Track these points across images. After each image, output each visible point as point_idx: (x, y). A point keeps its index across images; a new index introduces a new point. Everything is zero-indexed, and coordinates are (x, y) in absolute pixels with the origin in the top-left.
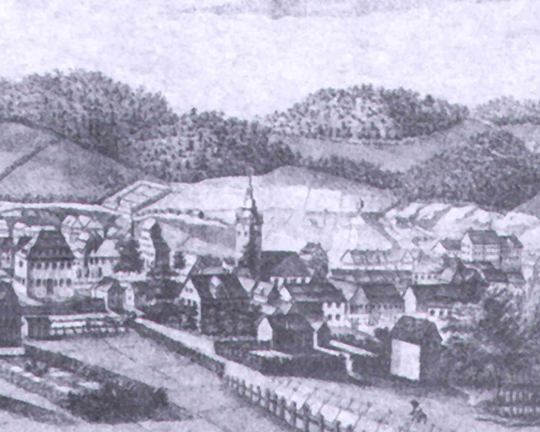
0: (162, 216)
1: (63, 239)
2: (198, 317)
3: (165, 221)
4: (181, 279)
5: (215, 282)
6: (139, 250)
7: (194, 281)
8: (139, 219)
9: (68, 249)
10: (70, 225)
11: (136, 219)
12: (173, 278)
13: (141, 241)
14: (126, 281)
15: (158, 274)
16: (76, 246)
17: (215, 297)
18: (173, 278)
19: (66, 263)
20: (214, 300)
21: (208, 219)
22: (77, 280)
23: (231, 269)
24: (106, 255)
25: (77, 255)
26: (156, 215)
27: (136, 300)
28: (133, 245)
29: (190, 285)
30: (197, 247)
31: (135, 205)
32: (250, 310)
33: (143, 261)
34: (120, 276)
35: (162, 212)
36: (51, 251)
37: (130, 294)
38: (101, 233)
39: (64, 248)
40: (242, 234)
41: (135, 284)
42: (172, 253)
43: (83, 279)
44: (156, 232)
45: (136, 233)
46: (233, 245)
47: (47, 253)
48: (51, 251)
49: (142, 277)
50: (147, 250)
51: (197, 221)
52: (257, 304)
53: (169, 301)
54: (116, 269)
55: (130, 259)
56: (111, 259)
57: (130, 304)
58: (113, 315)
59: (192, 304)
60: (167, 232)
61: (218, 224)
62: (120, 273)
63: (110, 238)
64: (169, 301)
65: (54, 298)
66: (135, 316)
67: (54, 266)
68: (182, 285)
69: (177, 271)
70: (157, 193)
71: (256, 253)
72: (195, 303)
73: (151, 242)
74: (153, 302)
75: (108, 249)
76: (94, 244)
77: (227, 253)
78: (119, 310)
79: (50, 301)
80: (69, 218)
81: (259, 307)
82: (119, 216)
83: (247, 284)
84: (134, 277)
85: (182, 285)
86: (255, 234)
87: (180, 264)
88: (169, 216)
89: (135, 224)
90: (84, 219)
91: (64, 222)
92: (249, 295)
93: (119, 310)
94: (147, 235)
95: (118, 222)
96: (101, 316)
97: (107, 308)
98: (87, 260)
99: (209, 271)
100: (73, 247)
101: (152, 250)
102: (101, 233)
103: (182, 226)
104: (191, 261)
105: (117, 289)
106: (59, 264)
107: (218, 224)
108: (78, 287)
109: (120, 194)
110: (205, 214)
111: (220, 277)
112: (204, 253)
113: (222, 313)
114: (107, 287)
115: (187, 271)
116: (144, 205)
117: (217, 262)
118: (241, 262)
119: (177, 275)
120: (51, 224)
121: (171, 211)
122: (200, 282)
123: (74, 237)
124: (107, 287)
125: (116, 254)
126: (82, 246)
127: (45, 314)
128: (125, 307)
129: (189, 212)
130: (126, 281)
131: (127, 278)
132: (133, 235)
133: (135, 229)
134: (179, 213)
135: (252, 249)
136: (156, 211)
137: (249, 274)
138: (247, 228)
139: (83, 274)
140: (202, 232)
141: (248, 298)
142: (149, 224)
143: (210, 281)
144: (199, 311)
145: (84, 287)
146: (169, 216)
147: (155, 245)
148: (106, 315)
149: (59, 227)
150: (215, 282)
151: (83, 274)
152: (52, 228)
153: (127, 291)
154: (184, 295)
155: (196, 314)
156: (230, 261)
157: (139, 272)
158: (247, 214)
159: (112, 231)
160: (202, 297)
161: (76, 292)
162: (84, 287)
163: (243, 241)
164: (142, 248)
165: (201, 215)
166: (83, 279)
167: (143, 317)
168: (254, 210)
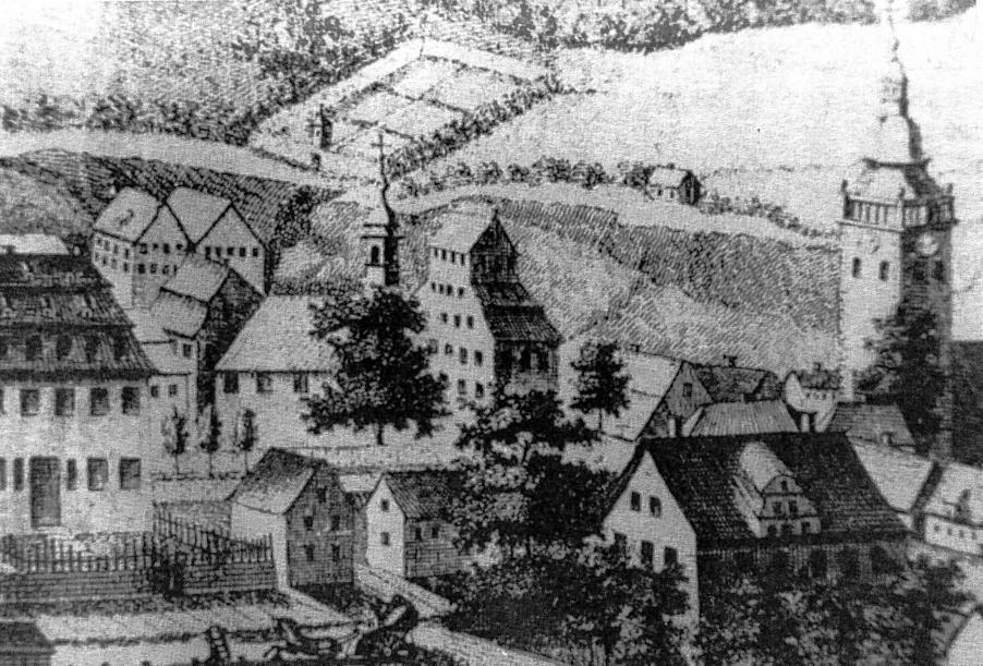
0: (520, 193)
1: (98, 288)
2: (688, 620)
3: (533, 214)
4: (609, 455)
5: (758, 465)
6: (419, 340)
7: (666, 468)
8: (423, 203)
9: (120, 334)
10: (132, 231)
11: (405, 207)
12: (572, 454)
13: (430, 303)
14: (366, 471)
15: (508, 435)
16: (156, 322)
17: (757, 528)
18: (572, 454)
19: (115, 389)
20: (753, 541)
21: (721, 206)
22: (167, 464)
23: (823, 408)
24: (276, 362)
25: (161, 357)
26: (489, 190)
27: (414, 550)
28: (392, 317)
29: (649, 480)
30: (682, 322)
31: (394, 143)
32: (911, 582)
33: (439, 385)
34: (345, 447)
35: (518, 173)
36: (49, 346)
37: (384, 521)
38: (250, 269)
39: (108, 328)
40: (870, 268)
41: (404, 480)
42: (568, 352)
43: (195, 460)
44: (494, 259)
45: (405, 266)
46: (828, 313)
47: (33, 349)
48: (49, 346)
49: (441, 449)
50: (457, 341)
51: (667, 214)
52: (936, 559)
53: (557, 551)
54: (323, 416)
55: (383, 368)
56: (299, 378)
57: (382, 562)
58: (308, 611)
59: (659, 565)
60: (543, 264)
61: (764, 229)
62: (342, 434)
63: (290, 290)
64: (557, 551)
65: (62, 537)
66: (411, 619)
67: (62, 403)
68: (613, 486)
69: (591, 421)
70: (500, 93)
71: (933, 345)
72: (670, 554)
73: (471, 305)
74: (489, 556)
75: (282, 335)
76: (226, 317)
77: (810, 349)
78: (340, 593)
79: (44, 553)
80: (132, 201)
81: (952, 571)
82: (330, 195)
83: (896, 476)
84: (404, 448)
85: (613, 486)
86: (923, 274)
87: (606, 387)
88: (551, 194)
89: (403, 227)
90: (195, 210)
91: (107, 219)
92: (908, 521)
93: (340, 593)
94: (460, 275)
95: (323, 216)
96: (259, 616)
97: (282, 584)
98: (211, 381)
99: (729, 420)
100: (145, 326)
101: (481, 337)
102: (250, 269)
103: (610, 241)
104: (648, 378)
105: (327, 501)
106: (82, 393)
107: (764, 229)
108: (171, 492)
109: (331, 96)
110: (708, 187)
111: (779, 444)
112: (700, 349)
113: (793, 600)
114: (281, 497)
115: (636, 415)
116: (447, 143)
117: (766, 388)
118: (866, 384)
119: (585, 436)
120: (44, 227)
121: (560, 172)
122: (698, 469)
123: (153, 281)
124: (281, 497)
125: (318, 355)
126: (190, 320)
127: (24, 608)
128: (363, 579)
129: (640, 177)
130: (366, 471)
131: (363, 455)
132: (392, 277)
133: (403, 251)
134: (595, 177)
135: (915, 326)
136: (492, 174)
137: (905, 435)
138: (891, 249)
139: (197, 434)
140: (702, 264)
141: (901, 535)
142: (461, 230)
143: (735, 463)
144: (691, 588)
145: (195, 491)
146: (551, 194)
147: (493, 314)
148: (280, 612)
149: (80, 242)
150: (758, 465)
151: (197, 434)
152: (51, 245)
153: (373, 512)
154: (621, 520)
155: (680, 603)
156: (823, 381)
157: (425, 429)
158: (889, 185)
159: (296, 261)
160: (706, 537)
161: (161, 509)
162: (195, 491)
163: (871, 299)
164: (435, 332)
165: (691, 189)
166: (195, 460)
167: (451, 622)
168: (915, 171)
